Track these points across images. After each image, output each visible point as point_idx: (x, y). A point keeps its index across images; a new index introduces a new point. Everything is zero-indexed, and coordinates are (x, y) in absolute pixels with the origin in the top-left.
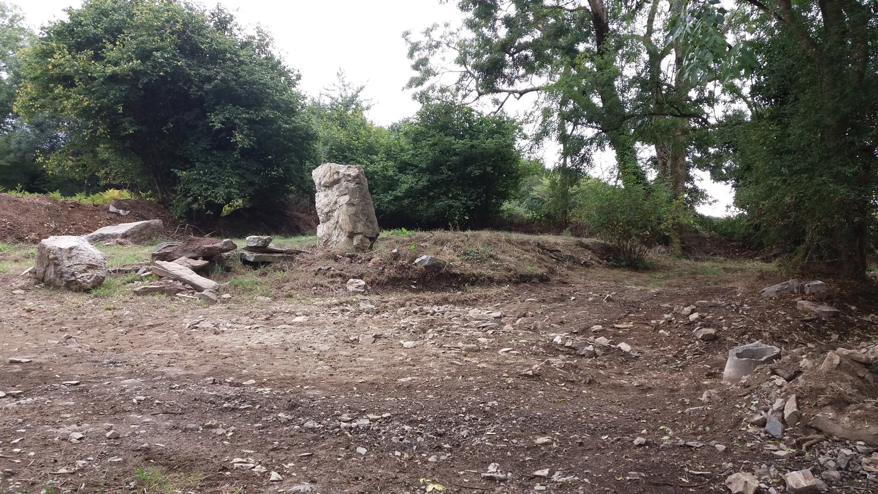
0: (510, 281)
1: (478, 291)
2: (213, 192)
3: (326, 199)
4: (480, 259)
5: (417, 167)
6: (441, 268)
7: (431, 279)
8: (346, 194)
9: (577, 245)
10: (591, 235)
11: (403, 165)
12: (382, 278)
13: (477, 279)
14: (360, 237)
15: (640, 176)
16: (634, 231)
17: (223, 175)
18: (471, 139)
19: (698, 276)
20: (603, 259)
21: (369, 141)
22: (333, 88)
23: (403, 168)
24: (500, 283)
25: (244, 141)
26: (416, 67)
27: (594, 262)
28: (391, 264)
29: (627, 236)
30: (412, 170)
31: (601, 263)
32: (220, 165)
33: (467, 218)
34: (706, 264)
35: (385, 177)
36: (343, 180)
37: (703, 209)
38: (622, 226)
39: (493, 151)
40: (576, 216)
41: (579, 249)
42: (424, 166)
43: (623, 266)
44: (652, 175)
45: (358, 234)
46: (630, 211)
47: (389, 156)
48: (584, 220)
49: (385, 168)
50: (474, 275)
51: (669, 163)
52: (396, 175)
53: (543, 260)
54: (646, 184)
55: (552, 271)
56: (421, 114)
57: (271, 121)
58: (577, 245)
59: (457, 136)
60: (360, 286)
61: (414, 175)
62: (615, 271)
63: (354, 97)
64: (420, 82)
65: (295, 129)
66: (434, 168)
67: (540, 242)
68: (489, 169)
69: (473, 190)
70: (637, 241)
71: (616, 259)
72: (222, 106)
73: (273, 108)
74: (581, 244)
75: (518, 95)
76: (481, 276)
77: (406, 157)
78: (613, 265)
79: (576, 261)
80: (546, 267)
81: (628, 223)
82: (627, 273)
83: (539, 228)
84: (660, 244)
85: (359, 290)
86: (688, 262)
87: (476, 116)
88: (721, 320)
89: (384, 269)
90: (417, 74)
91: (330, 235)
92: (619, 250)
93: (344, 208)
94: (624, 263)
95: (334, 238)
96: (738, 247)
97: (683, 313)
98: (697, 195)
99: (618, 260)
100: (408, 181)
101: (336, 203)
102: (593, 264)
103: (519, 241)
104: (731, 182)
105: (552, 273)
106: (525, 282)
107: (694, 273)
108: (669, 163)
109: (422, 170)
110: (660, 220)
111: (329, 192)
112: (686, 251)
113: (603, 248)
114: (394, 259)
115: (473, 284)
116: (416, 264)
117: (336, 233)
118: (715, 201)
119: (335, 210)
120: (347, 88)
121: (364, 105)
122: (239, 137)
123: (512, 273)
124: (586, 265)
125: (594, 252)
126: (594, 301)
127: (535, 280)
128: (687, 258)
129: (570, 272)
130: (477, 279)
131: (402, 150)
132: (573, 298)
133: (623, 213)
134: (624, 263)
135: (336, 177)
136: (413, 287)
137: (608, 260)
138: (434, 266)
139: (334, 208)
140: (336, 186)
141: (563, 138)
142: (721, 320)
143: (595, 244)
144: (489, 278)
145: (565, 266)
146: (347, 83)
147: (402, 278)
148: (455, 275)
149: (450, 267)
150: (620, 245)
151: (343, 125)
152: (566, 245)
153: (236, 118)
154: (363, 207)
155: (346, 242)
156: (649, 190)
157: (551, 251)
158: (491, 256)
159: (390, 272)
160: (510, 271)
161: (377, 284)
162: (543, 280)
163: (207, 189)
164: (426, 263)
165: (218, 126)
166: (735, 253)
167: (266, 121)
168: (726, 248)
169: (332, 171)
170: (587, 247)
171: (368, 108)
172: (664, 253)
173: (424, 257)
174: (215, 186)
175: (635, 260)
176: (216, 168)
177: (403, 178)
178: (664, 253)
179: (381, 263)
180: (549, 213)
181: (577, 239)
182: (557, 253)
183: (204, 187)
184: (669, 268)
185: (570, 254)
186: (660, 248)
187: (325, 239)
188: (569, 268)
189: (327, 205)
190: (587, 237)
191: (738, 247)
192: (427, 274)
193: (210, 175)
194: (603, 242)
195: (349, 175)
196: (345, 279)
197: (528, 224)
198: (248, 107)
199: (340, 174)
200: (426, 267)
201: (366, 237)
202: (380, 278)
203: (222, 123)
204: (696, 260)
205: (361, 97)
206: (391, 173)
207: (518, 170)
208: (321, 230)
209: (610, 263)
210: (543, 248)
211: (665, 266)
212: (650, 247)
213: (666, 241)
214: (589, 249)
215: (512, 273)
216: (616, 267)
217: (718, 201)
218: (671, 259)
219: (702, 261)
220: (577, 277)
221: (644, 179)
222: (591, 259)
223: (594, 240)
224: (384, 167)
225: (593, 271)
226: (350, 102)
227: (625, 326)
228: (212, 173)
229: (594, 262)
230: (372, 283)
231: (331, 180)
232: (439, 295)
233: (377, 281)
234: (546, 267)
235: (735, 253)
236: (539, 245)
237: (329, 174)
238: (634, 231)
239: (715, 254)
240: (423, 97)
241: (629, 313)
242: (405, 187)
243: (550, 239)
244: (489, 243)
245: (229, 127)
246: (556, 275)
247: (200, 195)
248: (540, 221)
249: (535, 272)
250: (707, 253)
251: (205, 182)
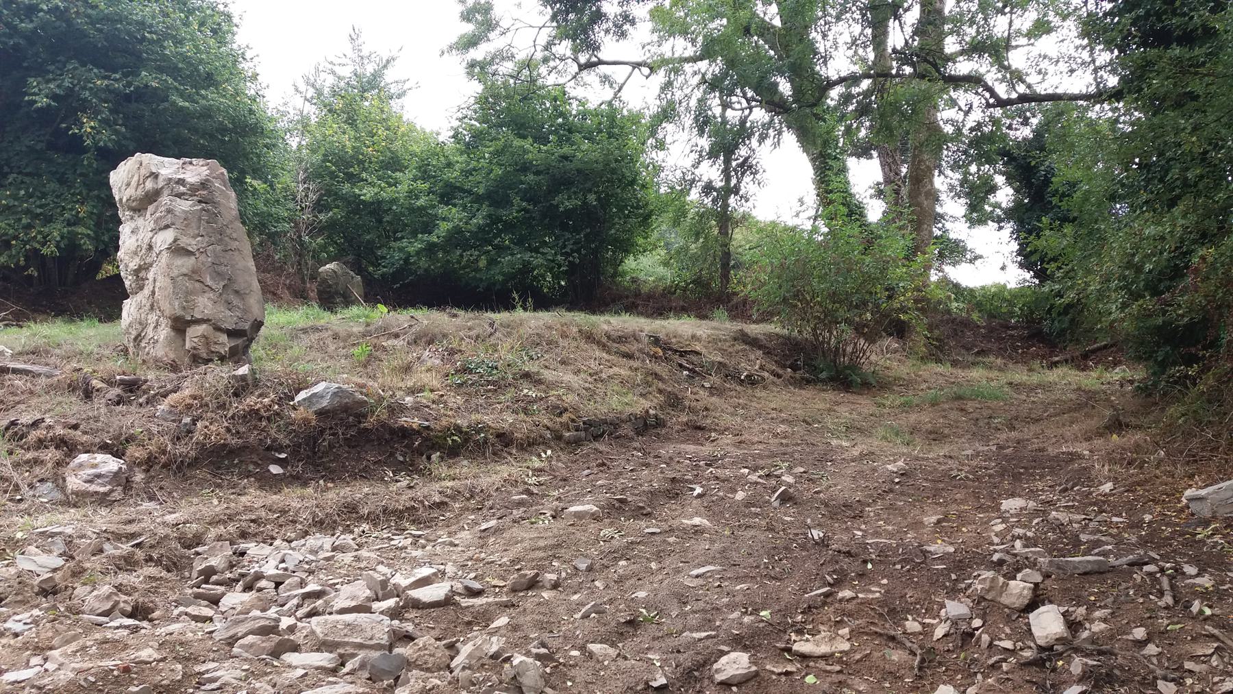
0: (558, 437)
1: (467, 474)
2: (40, 232)
3: (134, 238)
4: (494, 383)
5: (469, 192)
6: (365, 416)
7: (331, 446)
8: (167, 227)
9: (735, 339)
10: (765, 318)
11: (448, 189)
12: (184, 449)
13: (466, 441)
14: (201, 329)
15: (855, 211)
16: (842, 313)
17: (65, 200)
18: (560, 143)
19: (970, 406)
20: (784, 367)
21: (394, 147)
22: (344, 61)
23: (448, 194)
24: (529, 445)
25: (99, 132)
26: (467, 17)
27: (766, 374)
28: (222, 406)
29: (829, 320)
30: (463, 198)
31: (779, 376)
32: (62, 181)
33: (563, 283)
34: (976, 374)
35: (413, 210)
36: (166, 192)
37: (965, 275)
38: (819, 303)
39: (600, 166)
40: (744, 284)
41: (739, 347)
42: (481, 191)
43: (822, 381)
44: (875, 211)
45: (198, 322)
46: (837, 274)
47: (424, 173)
48: (746, 291)
49: (413, 195)
50: (458, 429)
51: (904, 191)
52: (434, 207)
53: (657, 376)
54: (864, 225)
55: (674, 402)
56: (482, 100)
57: (159, 96)
58: (735, 339)
59: (541, 139)
60: (99, 476)
61: (464, 208)
62: (807, 393)
63: (376, 75)
64: (471, 42)
65: (207, 113)
66: (496, 197)
67: (662, 336)
68: (592, 198)
69: (568, 235)
70: (849, 333)
71: (810, 366)
72: (60, 65)
73: (160, 70)
74: (743, 338)
75: (646, 71)
76: (478, 432)
77: (452, 175)
78: (803, 379)
79: (731, 375)
80: (660, 391)
81: (834, 297)
82: (830, 395)
83: (681, 303)
84: (890, 335)
85: (93, 488)
86: (940, 369)
87: (574, 108)
88: (1141, 644)
89: (194, 422)
90: (469, 28)
91: (145, 326)
92: (815, 348)
93: (163, 260)
94: (824, 375)
95: (150, 332)
96: (1022, 339)
97: (1005, 600)
98: (954, 251)
99: (814, 369)
100: (451, 218)
101: (150, 247)
102: (763, 379)
103: (615, 334)
104: (1009, 227)
105: (672, 406)
106: (596, 438)
107: (959, 398)
108: (904, 191)
109: (478, 199)
110: (891, 293)
111: (140, 222)
112: (937, 352)
113: (785, 344)
114: (236, 394)
115: (452, 453)
116: (294, 408)
117: (152, 318)
118: (976, 258)
119: (151, 265)
120: (366, 61)
121: (394, 89)
122: (88, 125)
123: (565, 418)
124: (751, 381)
125: (768, 352)
126: (748, 504)
127: (626, 430)
128: (938, 361)
129: (714, 399)
130: (466, 441)
131: (449, 165)
132: (699, 490)
133: (822, 278)
134: (824, 375)
135: (149, 185)
136: (275, 469)
137: (795, 368)
138: (346, 409)
139: (149, 260)
140: (151, 208)
141: (703, 123)
142: (1141, 644)
143: (770, 336)
144: (500, 436)
145: (707, 385)
146: (365, 53)
147: (244, 448)
148: (405, 434)
149: (396, 409)
150: (817, 339)
151: (351, 122)
152: (713, 341)
153: (84, 88)
154: (216, 256)
155: (170, 343)
156: (871, 238)
157: (683, 354)
158: (527, 376)
159: (212, 430)
160: (560, 414)
161: (165, 466)
162: (647, 426)
163: (29, 227)
164: (325, 403)
165: (42, 102)
166: (1015, 349)
167: (143, 95)
168: (1001, 339)
169: (143, 172)
170: (753, 342)
171: (399, 96)
172: (895, 351)
173: (319, 388)
174: (48, 220)
175: (846, 368)
176: (53, 186)
177: (442, 210)
178: (895, 351)
179: (189, 407)
180: (700, 277)
181: (737, 326)
182: (694, 358)
183: (24, 221)
184: (908, 384)
185: (719, 359)
186: (891, 343)
187: (134, 333)
188: (713, 390)
189: (136, 253)
190: (756, 322)
191: (1022, 339)
192: (322, 432)
193: (40, 198)
194: (786, 332)
195: (181, 182)
196: (69, 448)
197: (663, 295)
198: (110, 67)
199: (161, 178)
200: (321, 413)
201: (218, 329)
202: (181, 449)
203: (54, 97)
204: (955, 364)
205: (390, 76)
206: (422, 202)
207: (511, 147)
208: (129, 308)
209: (798, 376)
210: (666, 347)
211: (900, 378)
212: (871, 339)
213: (900, 330)
214: (760, 347)
215: (565, 418)
216: (808, 382)
217: (981, 257)
218: (909, 363)
219: (963, 368)
220: (724, 411)
221: (862, 215)
222: (762, 368)
223: (773, 328)
224: (410, 192)
225: (763, 394)
226: (370, 84)
227: (824, 649)
228: (44, 195)
229: (766, 374)
230: (149, 463)
231: (140, 192)
232: (336, 495)
233: (163, 459)
234: (660, 391)
235: (1015, 349)
236: (656, 341)
237: (136, 178)
238: (842, 313)
239: (982, 353)
240: (477, 69)
241: (838, 584)
242: (444, 227)
243: (682, 327)
244: (537, 342)
245: (70, 105)
246: (683, 410)
247: (16, 238)
248: (685, 289)
249: (629, 410)
250: (968, 350)
251: (28, 212)
